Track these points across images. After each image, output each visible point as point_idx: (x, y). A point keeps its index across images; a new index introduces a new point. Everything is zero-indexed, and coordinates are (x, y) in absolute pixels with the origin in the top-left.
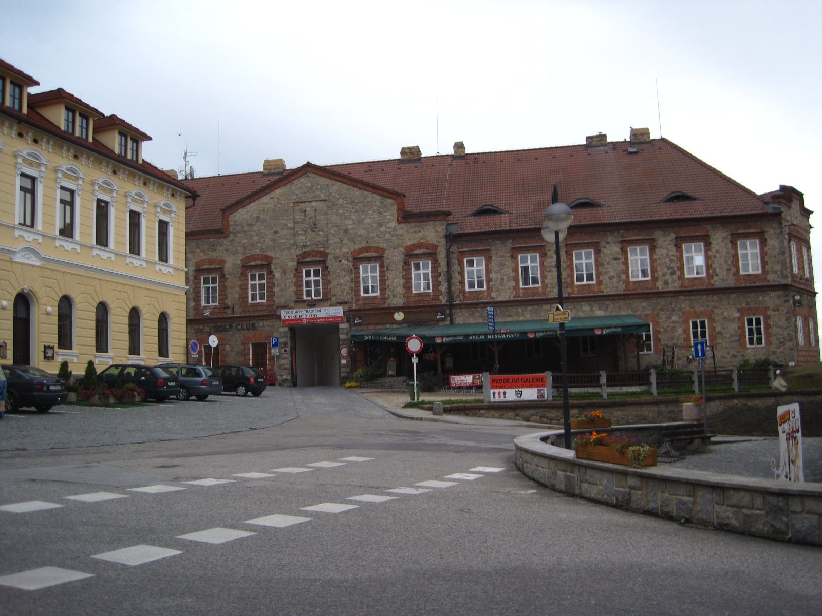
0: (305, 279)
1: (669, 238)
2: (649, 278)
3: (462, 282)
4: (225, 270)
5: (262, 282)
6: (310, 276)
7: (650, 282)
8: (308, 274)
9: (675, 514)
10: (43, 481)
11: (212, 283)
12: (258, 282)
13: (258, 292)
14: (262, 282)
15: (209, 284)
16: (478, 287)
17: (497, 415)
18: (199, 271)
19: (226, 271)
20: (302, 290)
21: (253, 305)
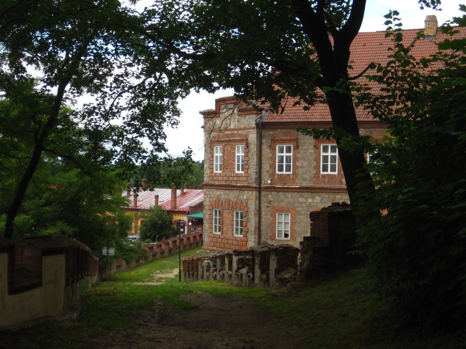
0: (322, 154)
1: (108, 78)
2: (336, 173)
3: (273, 166)
4: (249, 140)
5: (333, 154)
6: (282, 152)
7: (337, 176)
8: (281, 151)
9: (129, 237)
10: (260, 222)
11: (327, 156)
12: (285, 154)
13: (329, 164)
14: (333, 154)
15: (331, 156)
16: (331, 171)
17: (256, 226)
18: (212, 142)
19: (249, 141)
20: (234, 165)
21: (324, 176)
